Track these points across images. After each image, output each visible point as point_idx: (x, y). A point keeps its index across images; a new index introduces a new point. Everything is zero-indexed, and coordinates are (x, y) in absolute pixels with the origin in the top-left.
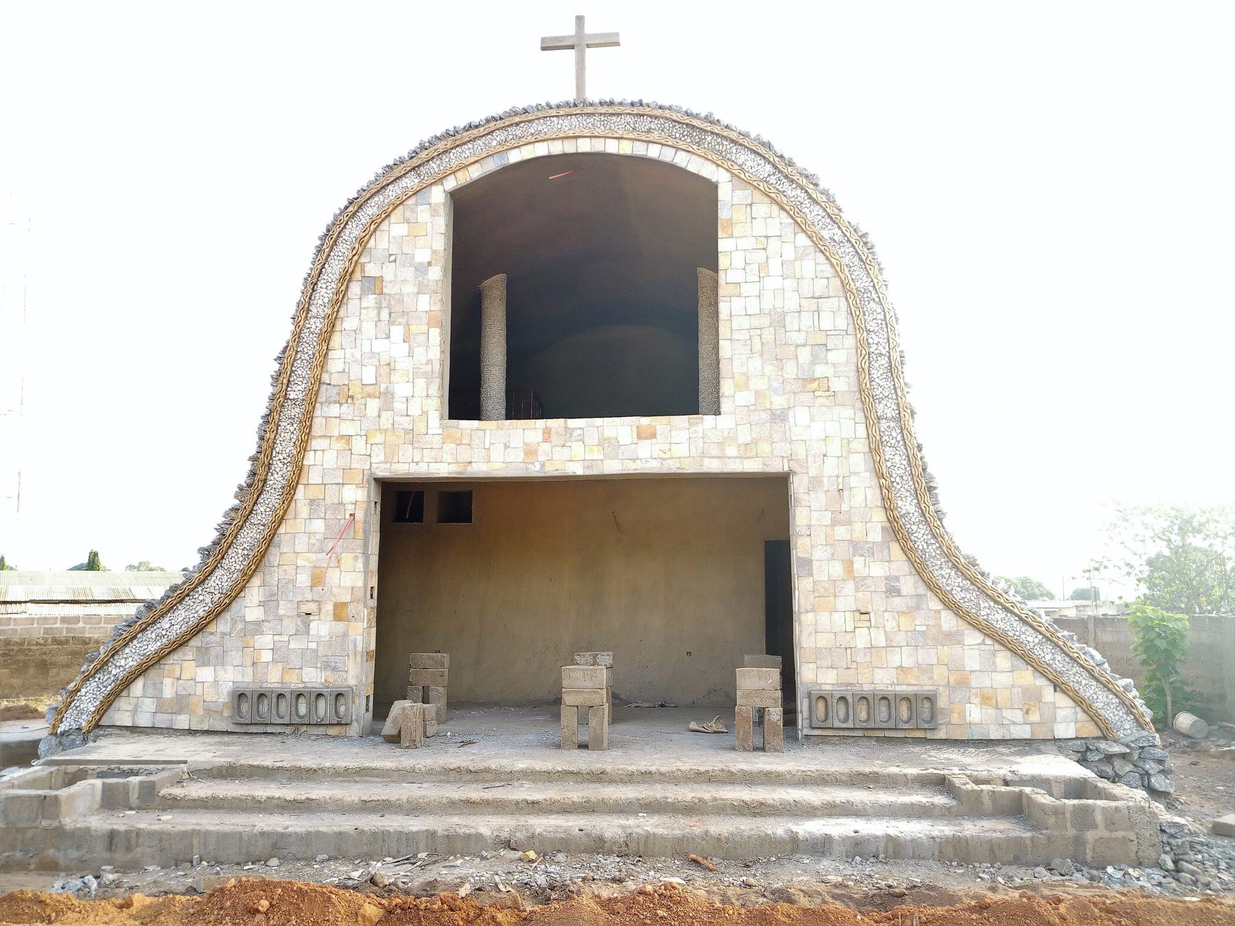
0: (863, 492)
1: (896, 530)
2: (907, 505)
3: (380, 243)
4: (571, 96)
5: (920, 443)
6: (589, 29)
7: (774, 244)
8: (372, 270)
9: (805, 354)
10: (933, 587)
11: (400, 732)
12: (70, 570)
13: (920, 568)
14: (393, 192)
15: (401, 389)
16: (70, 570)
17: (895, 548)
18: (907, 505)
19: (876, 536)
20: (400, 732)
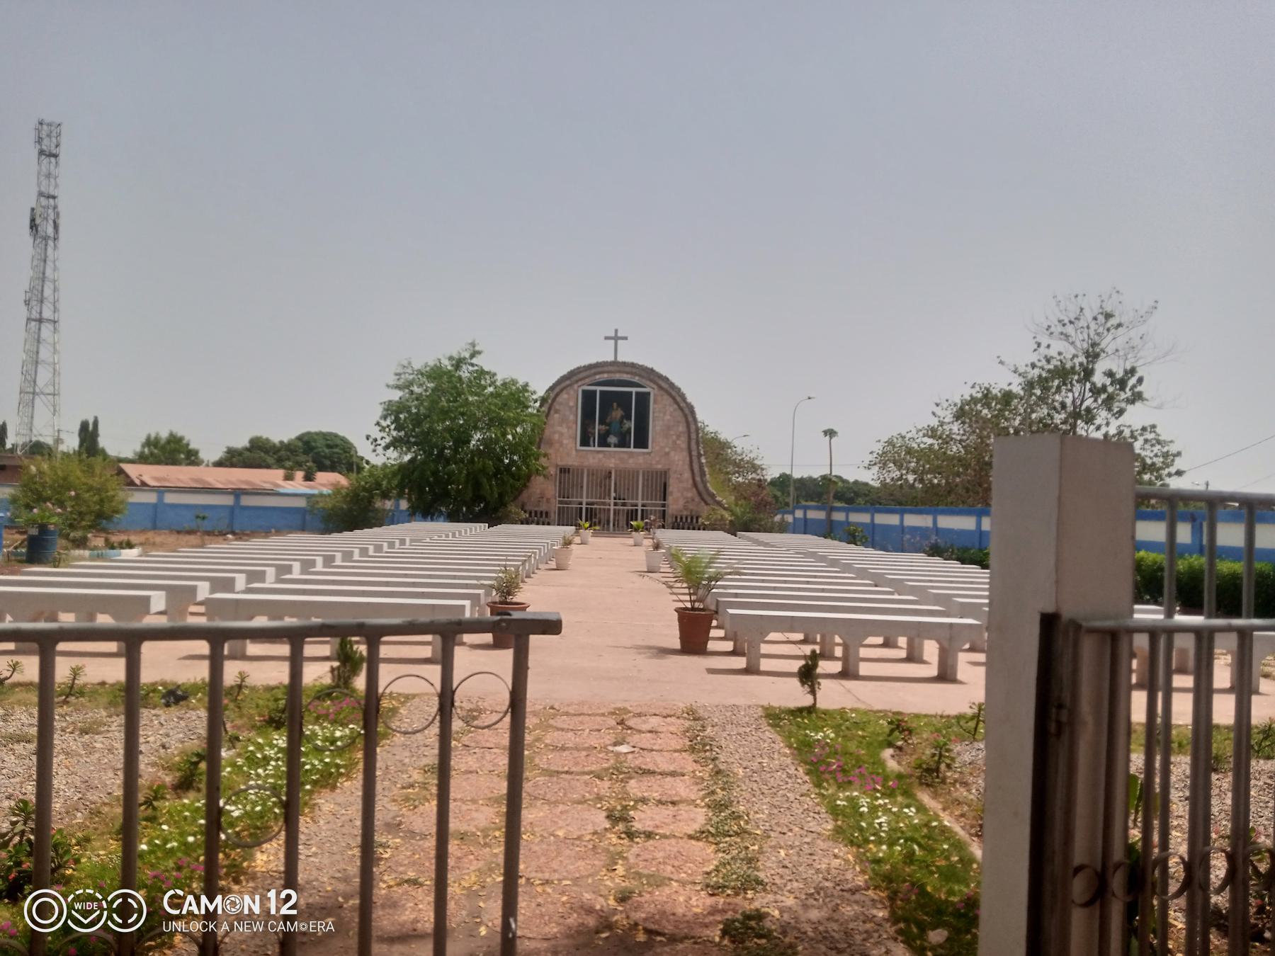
0: (687, 475)
1: (695, 484)
2: (698, 479)
3: (559, 399)
4: (613, 359)
5: (1140, 427)
6: (619, 335)
7: (667, 407)
8: (557, 407)
9: (674, 437)
10: (703, 499)
11: (961, 683)
12: (180, 659)
13: (700, 494)
14: (563, 385)
15: (565, 442)
16: (180, 659)
17: (694, 490)
18: (698, 479)
19: (690, 486)
20: (961, 683)
